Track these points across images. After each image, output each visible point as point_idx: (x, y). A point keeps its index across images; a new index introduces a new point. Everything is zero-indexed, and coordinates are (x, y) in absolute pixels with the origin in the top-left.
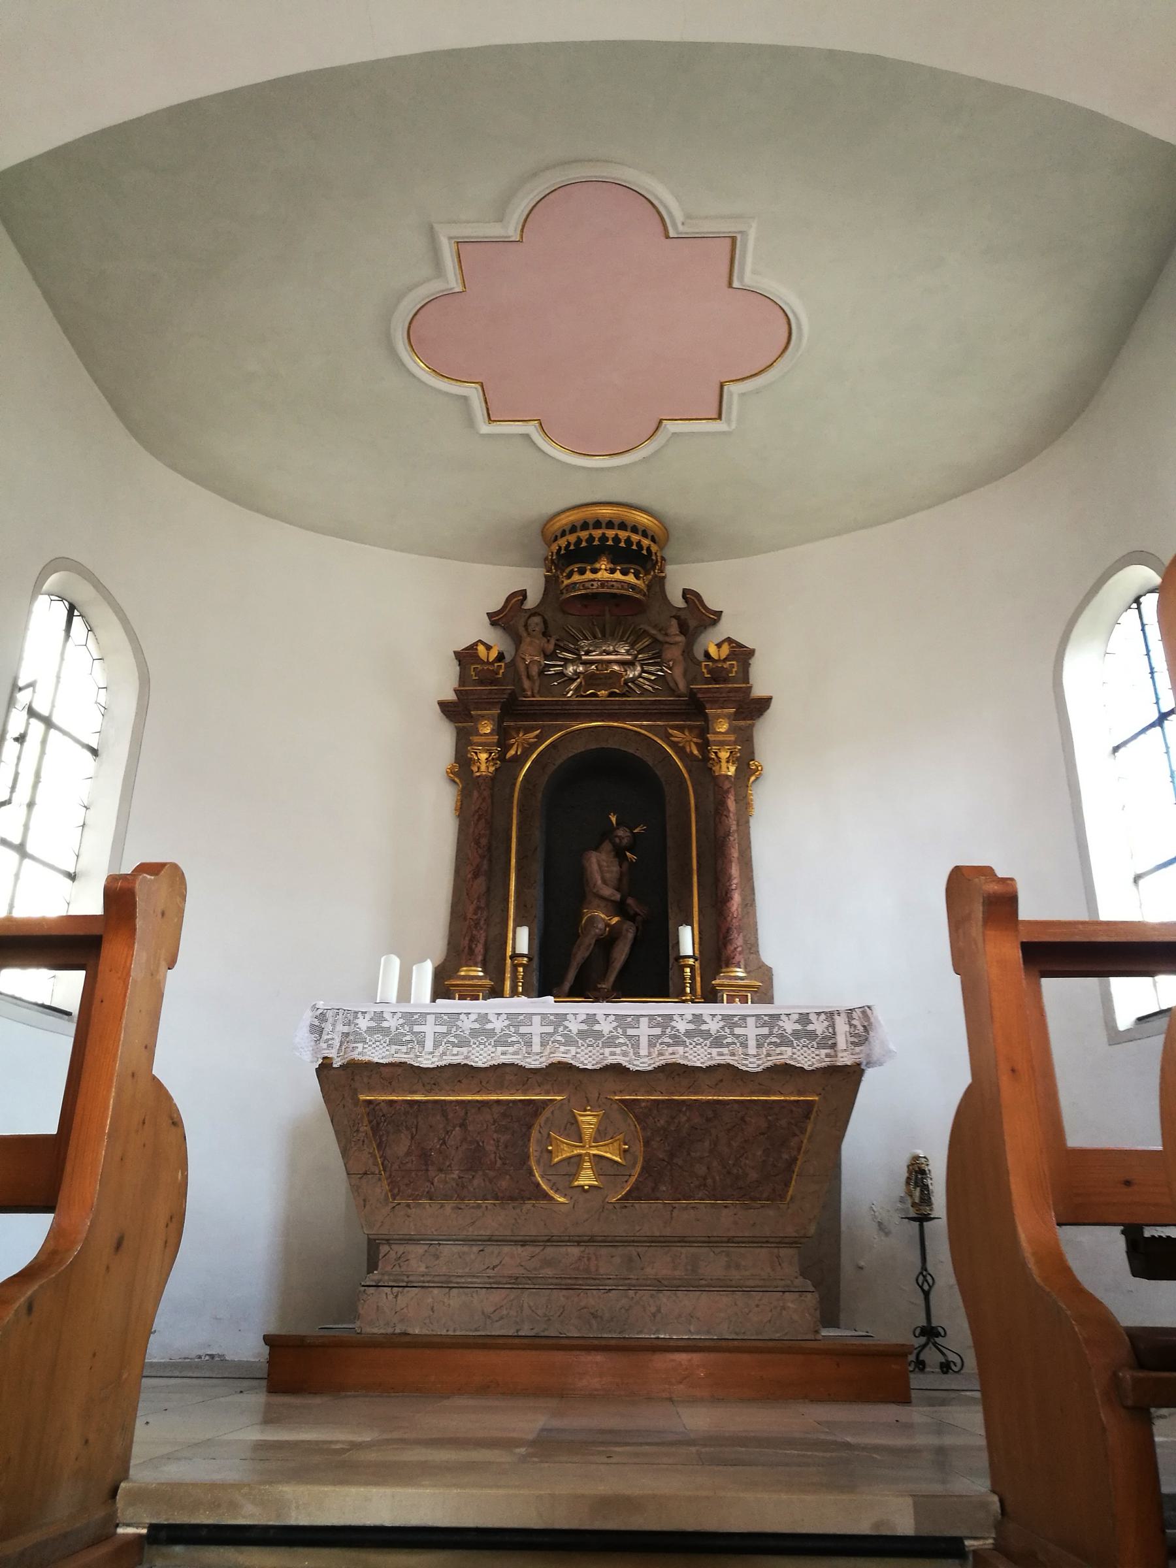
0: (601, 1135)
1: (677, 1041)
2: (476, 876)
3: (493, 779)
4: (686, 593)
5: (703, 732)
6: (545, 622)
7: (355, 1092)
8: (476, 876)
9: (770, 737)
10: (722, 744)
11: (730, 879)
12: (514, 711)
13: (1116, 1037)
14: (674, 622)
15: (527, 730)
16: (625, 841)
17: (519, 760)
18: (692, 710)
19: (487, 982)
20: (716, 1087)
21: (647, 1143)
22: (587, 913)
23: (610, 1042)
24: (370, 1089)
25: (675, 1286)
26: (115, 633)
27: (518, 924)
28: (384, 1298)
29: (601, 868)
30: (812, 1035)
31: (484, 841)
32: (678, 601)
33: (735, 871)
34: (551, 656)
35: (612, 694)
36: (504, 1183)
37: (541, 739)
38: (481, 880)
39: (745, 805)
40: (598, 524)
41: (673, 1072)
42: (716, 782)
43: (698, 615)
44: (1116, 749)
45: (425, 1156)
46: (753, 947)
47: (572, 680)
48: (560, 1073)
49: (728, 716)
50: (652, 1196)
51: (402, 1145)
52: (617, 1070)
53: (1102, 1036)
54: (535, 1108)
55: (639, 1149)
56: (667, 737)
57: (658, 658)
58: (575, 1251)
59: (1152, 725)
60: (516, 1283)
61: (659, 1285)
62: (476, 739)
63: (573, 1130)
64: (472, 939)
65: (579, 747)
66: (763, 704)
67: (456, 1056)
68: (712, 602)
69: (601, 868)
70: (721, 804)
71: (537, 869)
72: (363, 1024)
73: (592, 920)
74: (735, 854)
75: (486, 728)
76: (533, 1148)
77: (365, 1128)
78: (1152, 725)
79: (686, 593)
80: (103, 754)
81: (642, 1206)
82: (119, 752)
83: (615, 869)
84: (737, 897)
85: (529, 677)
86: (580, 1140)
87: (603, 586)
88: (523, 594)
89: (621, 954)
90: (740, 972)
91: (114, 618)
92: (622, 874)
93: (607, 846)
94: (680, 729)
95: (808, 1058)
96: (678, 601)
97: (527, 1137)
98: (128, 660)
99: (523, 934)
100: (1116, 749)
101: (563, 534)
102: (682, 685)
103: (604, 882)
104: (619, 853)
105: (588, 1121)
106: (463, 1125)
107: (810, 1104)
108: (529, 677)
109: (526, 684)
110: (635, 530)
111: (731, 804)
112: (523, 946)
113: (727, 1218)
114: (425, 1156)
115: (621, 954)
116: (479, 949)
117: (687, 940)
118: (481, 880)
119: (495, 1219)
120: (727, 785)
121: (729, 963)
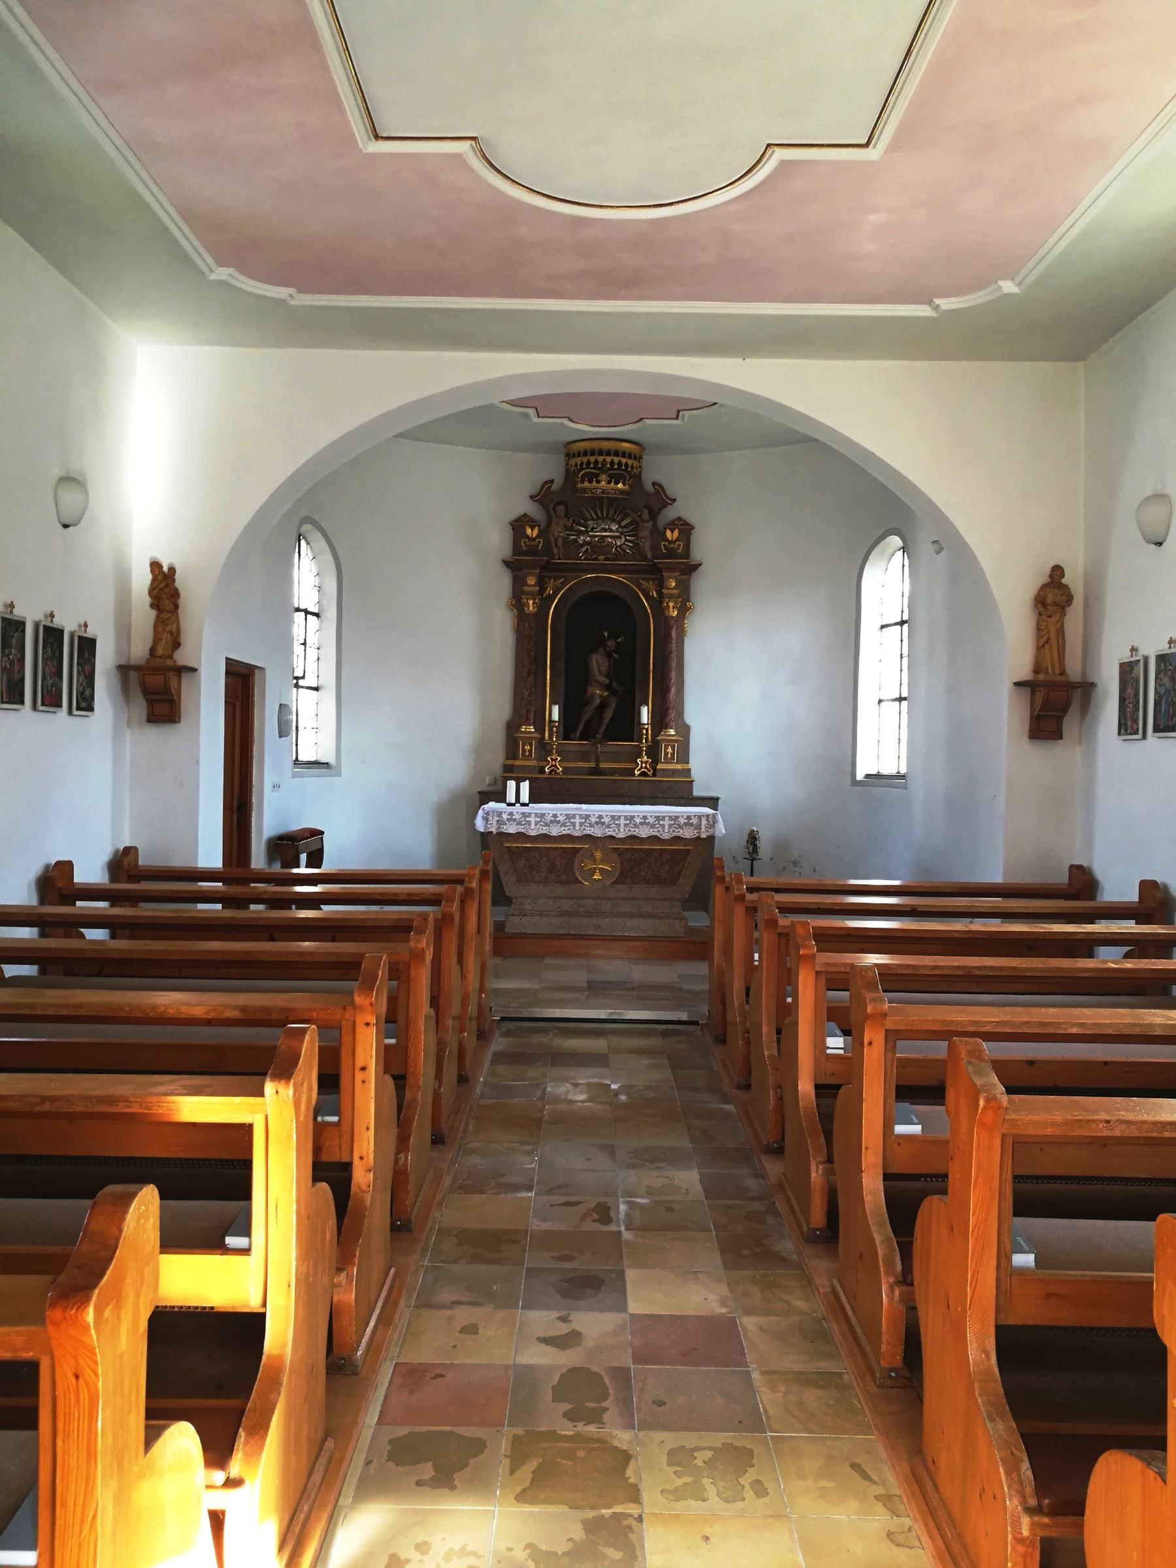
0: (602, 861)
1: (636, 826)
2: (529, 675)
3: (536, 614)
4: (654, 484)
5: (661, 585)
6: (566, 508)
7: (502, 843)
8: (529, 675)
9: (701, 585)
10: (671, 597)
11: (670, 679)
12: (549, 570)
13: (855, 783)
14: (646, 511)
15: (556, 579)
16: (613, 648)
17: (551, 598)
18: (656, 573)
19: (536, 735)
20: (652, 843)
21: (622, 864)
22: (590, 690)
23: (608, 826)
24: (508, 842)
25: (631, 916)
26: (323, 544)
27: (552, 703)
28: (516, 920)
29: (598, 663)
30: (692, 824)
31: (532, 654)
32: (650, 488)
33: (673, 675)
34: (571, 529)
35: (606, 559)
36: (564, 878)
37: (564, 584)
38: (532, 676)
39: (682, 633)
40: (601, 453)
41: (633, 838)
42: (667, 619)
43: (661, 498)
44: (883, 627)
45: (531, 867)
46: (681, 714)
47: (582, 545)
48: (588, 838)
49: (675, 578)
50: (623, 883)
51: (522, 863)
52: (612, 837)
53: (849, 780)
54: (577, 850)
55: (618, 865)
56: (639, 585)
57: (635, 532)
58: (592, 902)
59: (896, 624)
60: (569, 914)
61: (626, 915)
62: (526, 589)
63: (592, 858)
64: (528, 711)
65: (587, 590)
66: (696, 567)
67: (545, 830)
68: (671, 491)
69: (598, 663)
70: (668, 635)
71: (562, 666)
72: (505, 817)
73: (593, 694)
74: (674, 664)
75: (531, 581)
76: (576, 864)
77: (506, 856)
78: (896, 624)
79: (654, 484)
80: (323, 616)
81: (619, 886)
82: (331, 613)
83: (606, 664)
84: (673, 690)
85: (557, 546)
86: (595, 861)
87: (603, 492)
88: (552, 481)
89: (608, 715)
90: (672, 732)
91: (328, 550)
92: (610, 667)
93: (601, 650)
94: (647, 580)
95: (688, 833)
96: (650, 488)
97: (573, 861)
98: (329, 558)
99: (556, 710)
100: (883, 627)
101: (579, 455)
102: (649, 555)
103: (600, 674)
104: (609, 655)
105: (598, 855)
106: (547, 856)
107: (689, 850)
108: (557, 546)
109: (555, 551)
110: (624, 455)
111: (674, 634)
112: (556, 716)
113: (654, 891)
114: (531, 867)
115: (608, 715)
116: (532, 716)
117: (645, 715)
118: (532, 676)
119: (560, 890)
120: (672, 622)
121: (667, 727)
